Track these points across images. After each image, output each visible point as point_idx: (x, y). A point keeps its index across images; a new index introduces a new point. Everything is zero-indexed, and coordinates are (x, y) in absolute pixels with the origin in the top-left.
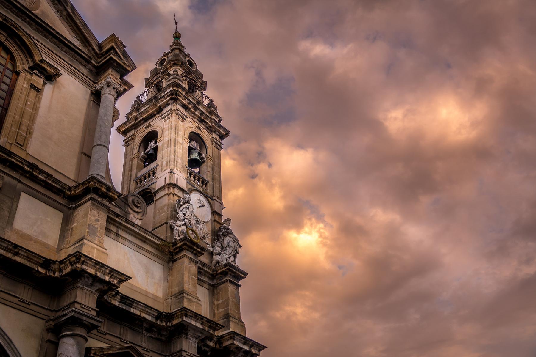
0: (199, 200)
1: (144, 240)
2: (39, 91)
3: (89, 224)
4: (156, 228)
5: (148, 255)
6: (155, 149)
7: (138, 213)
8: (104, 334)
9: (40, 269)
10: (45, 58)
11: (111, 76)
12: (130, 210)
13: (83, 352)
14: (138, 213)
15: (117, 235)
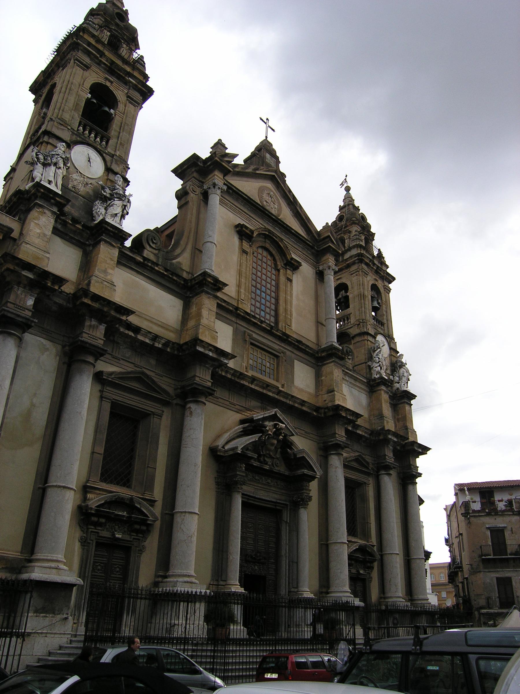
9: (315, 413)
10: (294, 256)
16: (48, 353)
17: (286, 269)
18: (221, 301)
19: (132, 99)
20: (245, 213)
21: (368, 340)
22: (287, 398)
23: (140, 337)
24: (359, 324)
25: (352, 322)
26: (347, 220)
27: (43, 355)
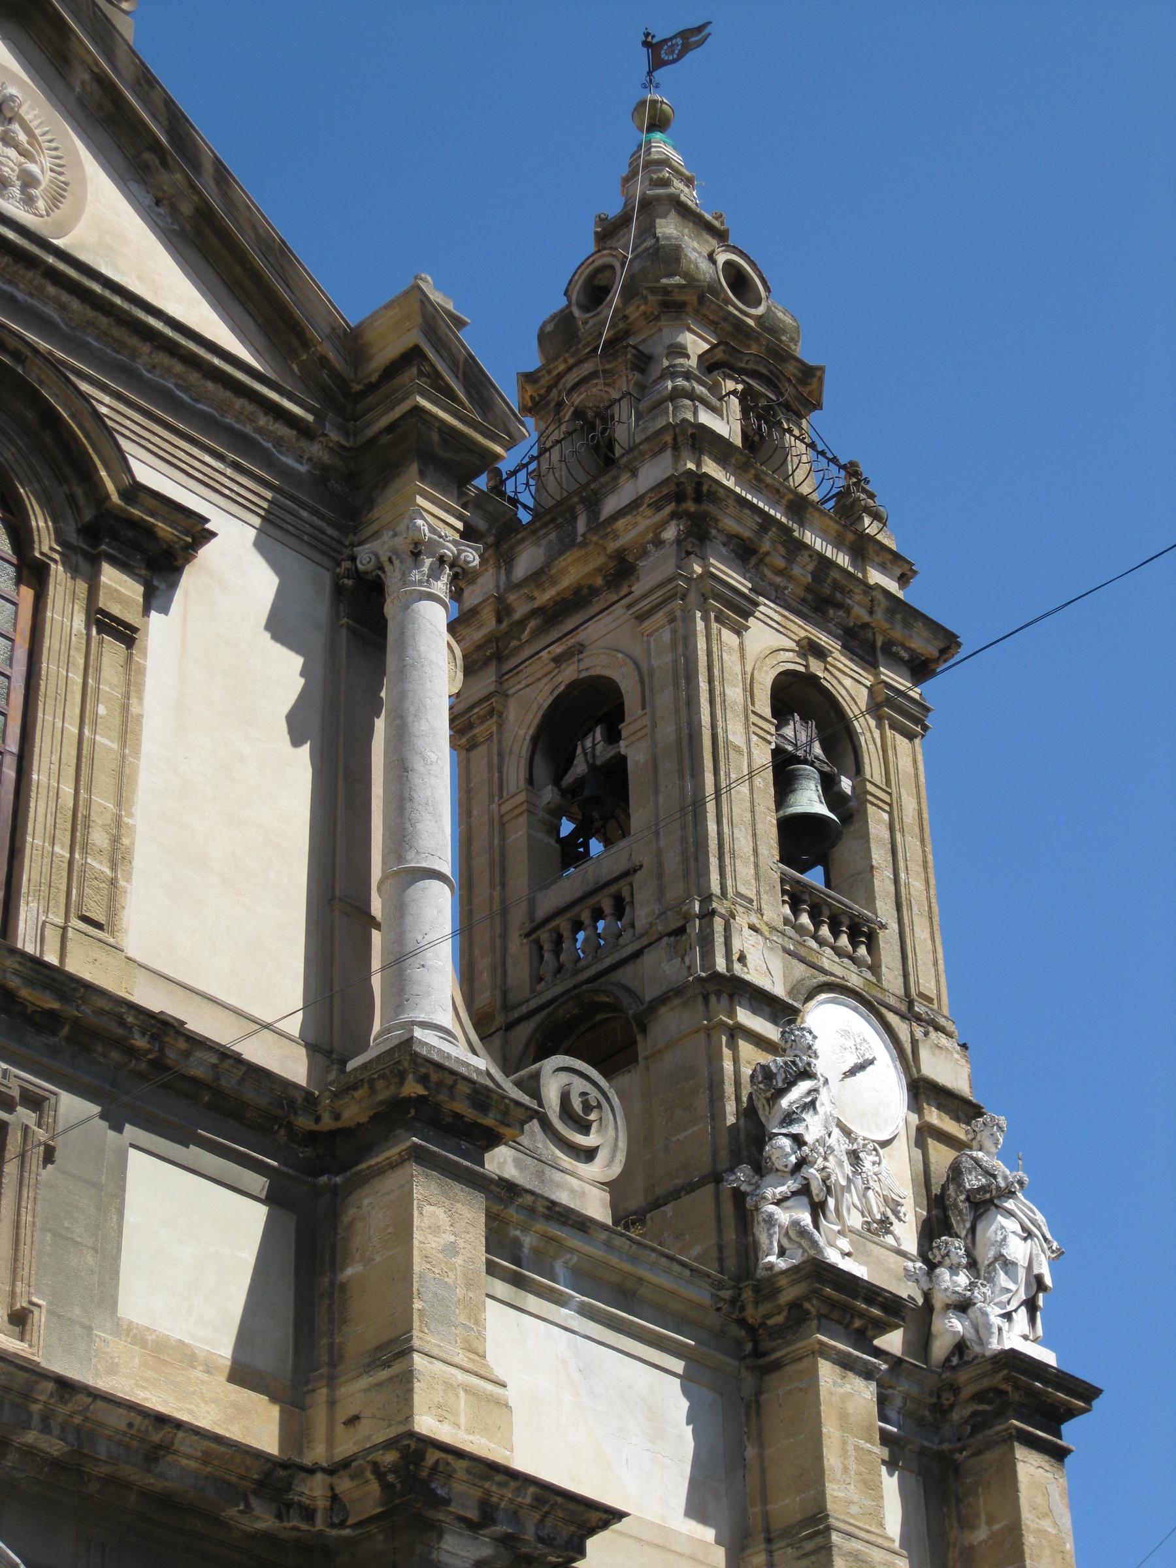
0: (846, 1033)
10: (148, 473)
17: (94, 562)
25: (641, 924)
26: (630, 293)
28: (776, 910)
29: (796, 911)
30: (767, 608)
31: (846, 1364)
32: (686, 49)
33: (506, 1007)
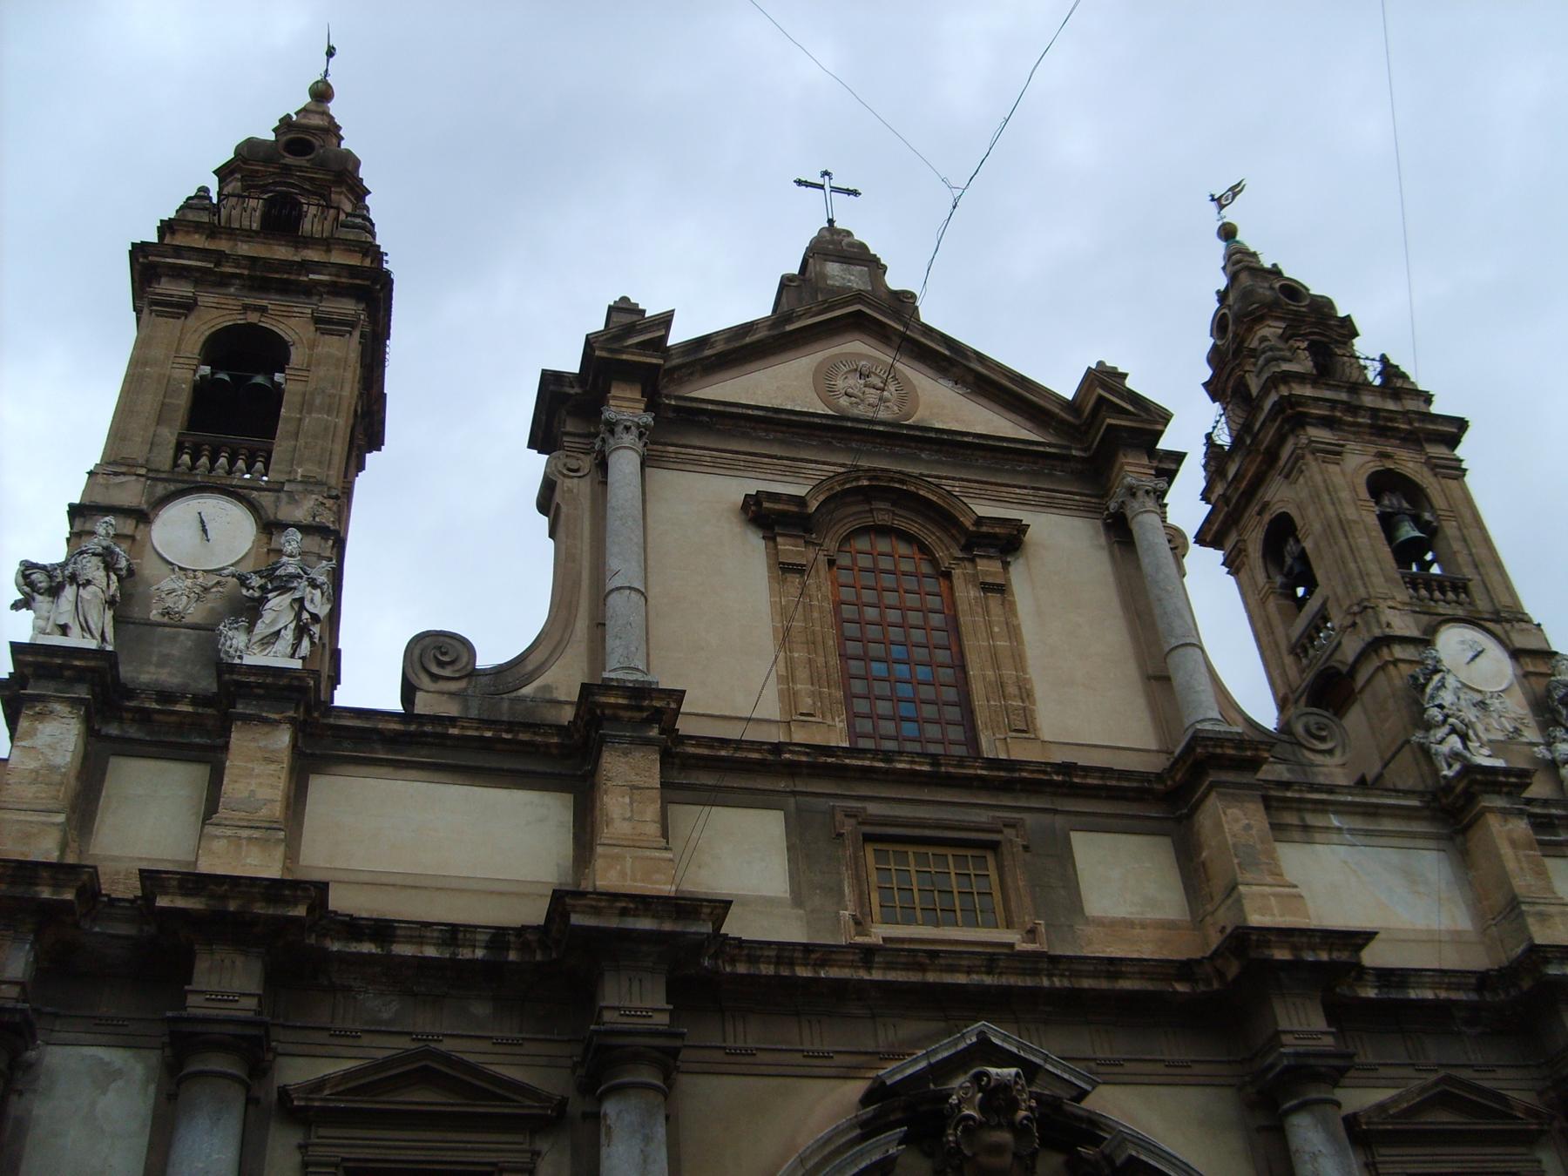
0: (1463, 642)
1: (1372, 812)
2: (1001, 589)
3: (1235, 845)
4: (1393, 756)
5: (1396, 841)
6: (1303, 557)
7: (1330, 752)
8: (1372, 1068)
9: (1180, 987)
10: (984, 509)
11: (1133, 470)
12: (1308, 754)
13: (1343, 1134)
14: (1330, 752)
15: (1306, 828)
16: (120, 1083)
17: (972, 560)
18: (712, 747)
19: (330, 322)
20: (816, 462)
21: (1396, 662)
22: (1036, 973)
23: (404, 950)
24: (1354, 624)
27: (104, 1093)
28: (1403, 594)
29: (1415, 589)
30: (1351, 446)
31: (1505, 813)
32: (1235, 195)
33: (1293, 692)
